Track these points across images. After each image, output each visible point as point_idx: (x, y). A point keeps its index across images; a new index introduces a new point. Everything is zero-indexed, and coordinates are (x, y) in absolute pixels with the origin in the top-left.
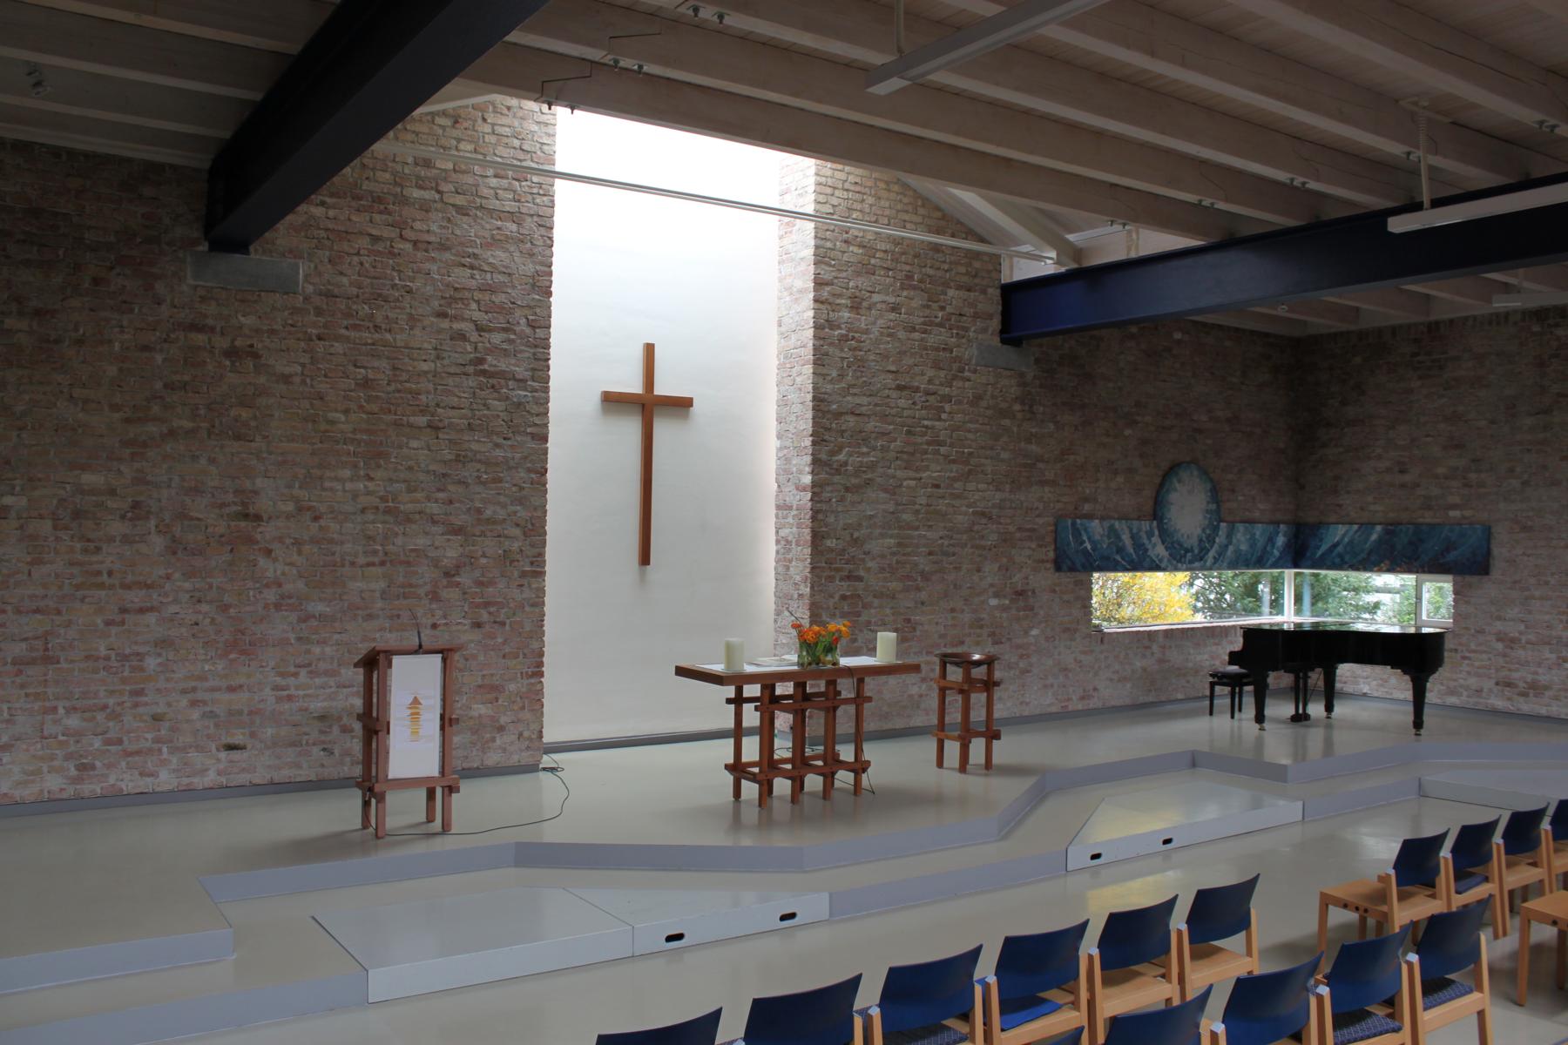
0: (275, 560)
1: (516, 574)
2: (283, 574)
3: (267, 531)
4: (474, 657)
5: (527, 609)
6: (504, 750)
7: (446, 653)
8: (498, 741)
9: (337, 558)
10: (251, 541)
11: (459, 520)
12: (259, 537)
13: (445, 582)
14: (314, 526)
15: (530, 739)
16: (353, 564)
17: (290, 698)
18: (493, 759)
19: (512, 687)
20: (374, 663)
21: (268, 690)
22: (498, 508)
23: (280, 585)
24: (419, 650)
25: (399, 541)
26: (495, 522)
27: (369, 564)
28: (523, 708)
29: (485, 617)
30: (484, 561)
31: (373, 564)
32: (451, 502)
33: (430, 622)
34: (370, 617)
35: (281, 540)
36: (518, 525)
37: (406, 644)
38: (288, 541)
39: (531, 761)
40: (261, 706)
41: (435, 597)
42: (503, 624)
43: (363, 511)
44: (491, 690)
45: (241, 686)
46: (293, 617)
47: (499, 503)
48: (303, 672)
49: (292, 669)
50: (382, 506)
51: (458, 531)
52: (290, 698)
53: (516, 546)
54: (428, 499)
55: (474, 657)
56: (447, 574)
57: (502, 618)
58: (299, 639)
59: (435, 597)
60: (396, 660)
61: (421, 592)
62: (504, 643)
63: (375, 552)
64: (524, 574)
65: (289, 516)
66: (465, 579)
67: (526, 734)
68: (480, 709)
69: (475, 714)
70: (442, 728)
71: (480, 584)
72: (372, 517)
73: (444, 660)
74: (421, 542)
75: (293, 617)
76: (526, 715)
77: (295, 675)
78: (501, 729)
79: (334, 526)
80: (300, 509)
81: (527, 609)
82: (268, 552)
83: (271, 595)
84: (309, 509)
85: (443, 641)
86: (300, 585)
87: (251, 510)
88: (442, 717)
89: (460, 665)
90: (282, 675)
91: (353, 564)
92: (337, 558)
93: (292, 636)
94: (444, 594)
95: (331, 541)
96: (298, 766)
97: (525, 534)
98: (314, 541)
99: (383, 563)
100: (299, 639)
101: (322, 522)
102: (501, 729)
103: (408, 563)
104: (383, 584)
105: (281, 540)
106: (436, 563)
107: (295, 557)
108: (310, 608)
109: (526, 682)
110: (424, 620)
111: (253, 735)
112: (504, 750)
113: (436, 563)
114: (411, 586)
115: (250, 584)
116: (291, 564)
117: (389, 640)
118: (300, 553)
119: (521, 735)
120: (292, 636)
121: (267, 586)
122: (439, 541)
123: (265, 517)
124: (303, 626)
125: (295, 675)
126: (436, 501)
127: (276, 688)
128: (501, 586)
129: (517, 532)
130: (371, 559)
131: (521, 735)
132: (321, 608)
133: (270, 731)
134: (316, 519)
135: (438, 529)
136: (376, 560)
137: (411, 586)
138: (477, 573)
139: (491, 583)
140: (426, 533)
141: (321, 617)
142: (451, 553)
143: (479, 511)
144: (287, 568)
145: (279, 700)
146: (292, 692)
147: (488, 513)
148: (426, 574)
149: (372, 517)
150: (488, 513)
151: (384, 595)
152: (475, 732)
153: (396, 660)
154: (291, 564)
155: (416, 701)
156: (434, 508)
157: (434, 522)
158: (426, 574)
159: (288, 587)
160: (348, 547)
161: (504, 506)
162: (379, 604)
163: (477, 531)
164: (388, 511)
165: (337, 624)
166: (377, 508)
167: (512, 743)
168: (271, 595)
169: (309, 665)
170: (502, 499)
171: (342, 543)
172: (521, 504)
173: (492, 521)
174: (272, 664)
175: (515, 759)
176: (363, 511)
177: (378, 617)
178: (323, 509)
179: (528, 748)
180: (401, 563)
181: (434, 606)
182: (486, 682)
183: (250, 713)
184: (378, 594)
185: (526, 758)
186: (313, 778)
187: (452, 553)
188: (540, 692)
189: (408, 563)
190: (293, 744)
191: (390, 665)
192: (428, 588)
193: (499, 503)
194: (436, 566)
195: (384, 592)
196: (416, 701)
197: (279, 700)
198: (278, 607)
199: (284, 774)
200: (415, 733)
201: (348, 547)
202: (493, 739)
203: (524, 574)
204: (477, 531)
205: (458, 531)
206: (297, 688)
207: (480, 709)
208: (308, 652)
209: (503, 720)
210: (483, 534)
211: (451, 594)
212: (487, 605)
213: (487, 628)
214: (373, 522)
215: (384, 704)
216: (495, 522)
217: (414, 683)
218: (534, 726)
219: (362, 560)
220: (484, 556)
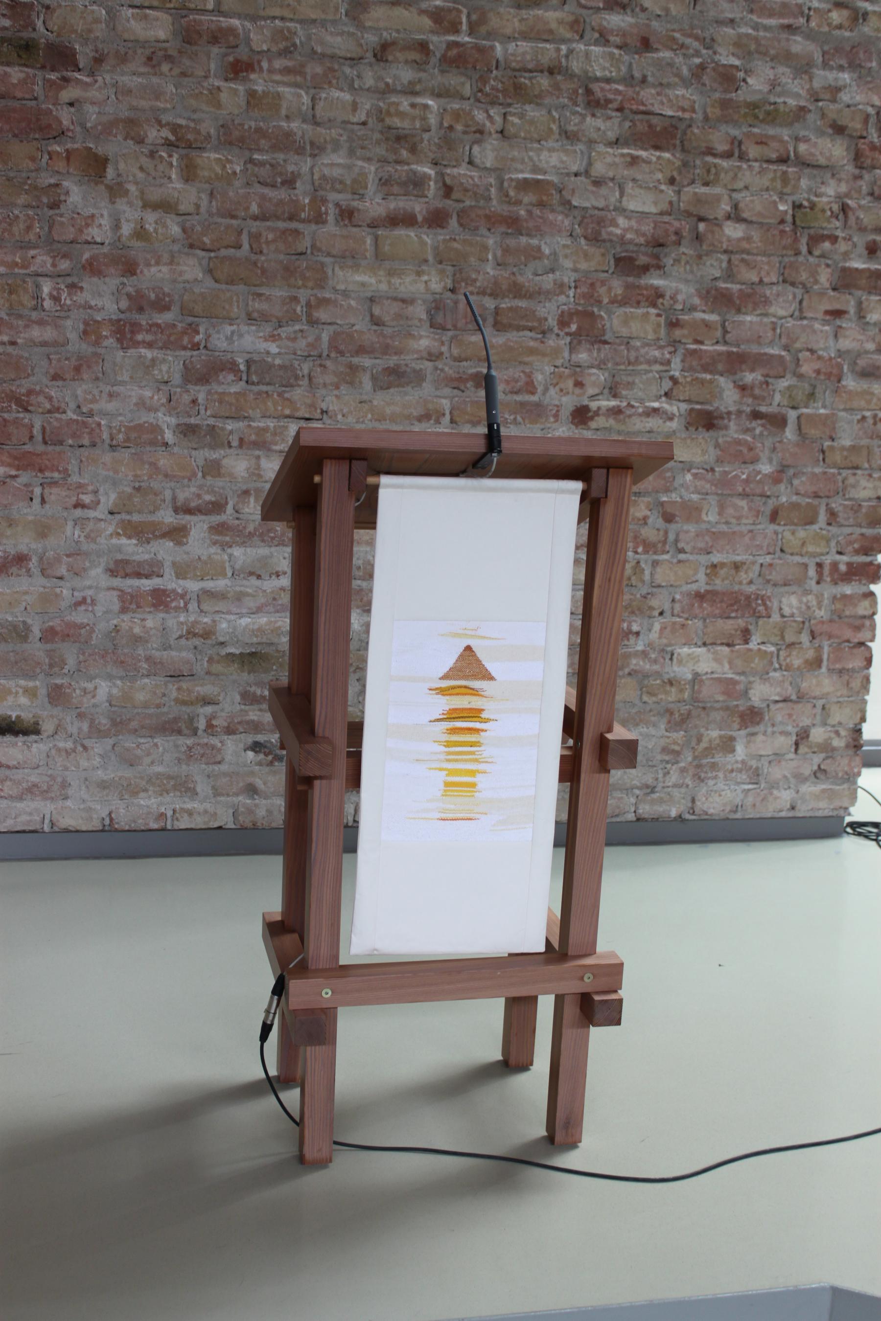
0: (116, 191)
1: (825, 277)
2: (140, 233)
3: (91, 101)
4: (692, 512)
5: (850, 382)
6: (756, 775)
7: (600, 479)
8: (740, 750)
9: (302, 194)
10: (40, 128)
11: (673, 100)
12: (65, 117)
13: (617, 286)
14: (233, 96)
15: (827, 749)
16: (347, 215)
17: (160, 599)
18: (719, 797)
19: (791, 603)
20: (321, 501)
21: (97, 575)
22: (784, 73)
23: (130, 269)
24: (488, 459)
25: (488, 153)
26: (773, 116)
27: (395, 220)
28: (816, 663)
29: (728, 397)
30: (733, 231)
31: (408, 220)
32: (646, 44)
33: (569, 402)
34: (395, 377)
35: (131, 127)
36: (839, 130)
37: (440, 433)
38: (153, 134)
39: (824, 807)
40: (80, 617)
41: (585, 327)
42: (778, 422)
43: (382, 53)
44: (733, 608)
45: (21, 559)
46: (171, 365)
47: (787, 58)
48: (199, 528)
49: (167, 517)
50: (438, 42)
51: (663, 135)
52: (160, 599)
53: (830, 191)
54: (579, 28)
55: (692, 512)
56: (626, 264)
57: (776, 403)
58: (187, 431)
59: (585, 327)
60: (396, 495)
61: (549, 311)
62: (776, 479)
63: (417, 183)
64: (846, 281)
65: (155, 57)
66: (676, 283)
67: (818, 734)
68: (698, 661)
69: (685, 673)
70: (570, 770)
71: (718, 299)
72: (406, 75)
73: (592, 508)
74: (553, 160)
75: (171, 365)
76: (823, 683)
77: (177, 534)
78: (751, 717)
79: (294, 97)
80: (189, 36)
81: (850, 382)
82: (95, 166)
83: (104, 297)
84: (216, 37)
85: (593, 440)
86: (191, 269)
87: (41, 31)
88: (573, 723)
89: (649, 533)
90: (141, 532)
91: (347, 215)
92: (302, 194)
93: (167, 422)
94: (615, 321)
95: (286, 142)
96: (185, 787)
97: (857, 157)
98: (231, 138)
99: (437, 219)
100: (187, 431)
101: (259, 83)
102: (751, 717)
103: (513, 224)
104: (435, 282)
105: (131, 127)
106: (593, 229)
107: (177, 184)
108: (219, 342)
109: (829, 590)
110: (553, 397)
111: (57, 696)
112: (756, 775)
113: (593, 229)
114: (517, 291)
115: (42, 260)
116: (166, 206)
117: (351, 414)
118: (189, 173)
119: (802, 736)
120: (167, 422)
121: (93, 268)
122: (606, 161)
123: (84, 54)
124: (201, 393)
125: (177, 534)
126: (603, 38)
127: (121, 568)
128: (779, 309)
129: (836, 151)
130: (400, 204)
131: (802, 736)
132: (250, 342)
133: (104, 689)
134: (239, 69)
135: (604, 125)
136: (418, 208)
137: (517, 291)
138: (713, 268)
139: (752, 298)
140: (569, 136)
141: (256, 370)
142: (640, 202)
143: (729, 78)
144: (151, 218)
145: (129, 602)
146: (168, 582)
147: (756, 85)
148: (562, 259)
149: (406, 75)
150: (756, 85)
151: (437, 316)
152: (679, 721)
153: (396, 495)
154: (166, 206)
155: (469, 667)
156: (597, 60)
157: (594, 104)
158: (562, 259)
159: (155, 275)
160: (334, 163)
161: (804, 68)
162: (425, 342)
163: (719, 140)
164: (456, 59)
165: (298, 394)
166: (423, 47)
167: (778, 757)
168: (104, 297)
169: (217, 507)
170: (798, 45)
171: (317, 149)
172: (854, 65)
173: (764, 112)
174: (108, 499)
175: (780, 802)
176: (382, 53)
177: (419, 378)
178: (259, 39)
179: (819, 773)
180: (492, 221)
181: (583, 356)
182: (719, 585)
183: (49, 635)
184: (419, 311)
185: (813, 800)
186: (225, 819)
187: (641, 203)
188: (865, 623)
189: (513, 224)
190: (170, 727)
191: (367, 515)
192: (568, 300)
193: (787, 58)
194: (595, 239)
195: (436, 307)
196: (469, 667)
197: (129, 602)
198: (125, 333)
199: (146, 808)
200: (459, 787)
201: (334, 163)
202: (728, 744)
203: (846, 281)
204: (719, 140)
205: (663, 135)
206: (181, 572)
207: (698, 661)
208: (213, 469)
209: (760, 693)
210: (736, 151)
211: (637, 325)
212: (736, 362)
213: (733, 431)
214: (410, 91)
215: (352, 663)
216: (773, 116)
217: (469, 579)
218: (842, 716)
219: (375, 205)
220: (736, 215)
